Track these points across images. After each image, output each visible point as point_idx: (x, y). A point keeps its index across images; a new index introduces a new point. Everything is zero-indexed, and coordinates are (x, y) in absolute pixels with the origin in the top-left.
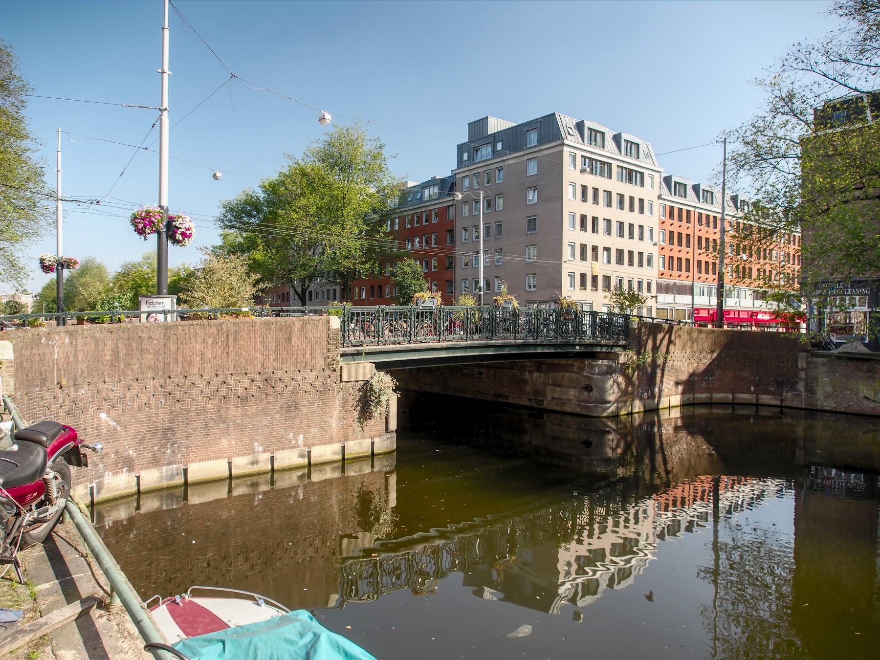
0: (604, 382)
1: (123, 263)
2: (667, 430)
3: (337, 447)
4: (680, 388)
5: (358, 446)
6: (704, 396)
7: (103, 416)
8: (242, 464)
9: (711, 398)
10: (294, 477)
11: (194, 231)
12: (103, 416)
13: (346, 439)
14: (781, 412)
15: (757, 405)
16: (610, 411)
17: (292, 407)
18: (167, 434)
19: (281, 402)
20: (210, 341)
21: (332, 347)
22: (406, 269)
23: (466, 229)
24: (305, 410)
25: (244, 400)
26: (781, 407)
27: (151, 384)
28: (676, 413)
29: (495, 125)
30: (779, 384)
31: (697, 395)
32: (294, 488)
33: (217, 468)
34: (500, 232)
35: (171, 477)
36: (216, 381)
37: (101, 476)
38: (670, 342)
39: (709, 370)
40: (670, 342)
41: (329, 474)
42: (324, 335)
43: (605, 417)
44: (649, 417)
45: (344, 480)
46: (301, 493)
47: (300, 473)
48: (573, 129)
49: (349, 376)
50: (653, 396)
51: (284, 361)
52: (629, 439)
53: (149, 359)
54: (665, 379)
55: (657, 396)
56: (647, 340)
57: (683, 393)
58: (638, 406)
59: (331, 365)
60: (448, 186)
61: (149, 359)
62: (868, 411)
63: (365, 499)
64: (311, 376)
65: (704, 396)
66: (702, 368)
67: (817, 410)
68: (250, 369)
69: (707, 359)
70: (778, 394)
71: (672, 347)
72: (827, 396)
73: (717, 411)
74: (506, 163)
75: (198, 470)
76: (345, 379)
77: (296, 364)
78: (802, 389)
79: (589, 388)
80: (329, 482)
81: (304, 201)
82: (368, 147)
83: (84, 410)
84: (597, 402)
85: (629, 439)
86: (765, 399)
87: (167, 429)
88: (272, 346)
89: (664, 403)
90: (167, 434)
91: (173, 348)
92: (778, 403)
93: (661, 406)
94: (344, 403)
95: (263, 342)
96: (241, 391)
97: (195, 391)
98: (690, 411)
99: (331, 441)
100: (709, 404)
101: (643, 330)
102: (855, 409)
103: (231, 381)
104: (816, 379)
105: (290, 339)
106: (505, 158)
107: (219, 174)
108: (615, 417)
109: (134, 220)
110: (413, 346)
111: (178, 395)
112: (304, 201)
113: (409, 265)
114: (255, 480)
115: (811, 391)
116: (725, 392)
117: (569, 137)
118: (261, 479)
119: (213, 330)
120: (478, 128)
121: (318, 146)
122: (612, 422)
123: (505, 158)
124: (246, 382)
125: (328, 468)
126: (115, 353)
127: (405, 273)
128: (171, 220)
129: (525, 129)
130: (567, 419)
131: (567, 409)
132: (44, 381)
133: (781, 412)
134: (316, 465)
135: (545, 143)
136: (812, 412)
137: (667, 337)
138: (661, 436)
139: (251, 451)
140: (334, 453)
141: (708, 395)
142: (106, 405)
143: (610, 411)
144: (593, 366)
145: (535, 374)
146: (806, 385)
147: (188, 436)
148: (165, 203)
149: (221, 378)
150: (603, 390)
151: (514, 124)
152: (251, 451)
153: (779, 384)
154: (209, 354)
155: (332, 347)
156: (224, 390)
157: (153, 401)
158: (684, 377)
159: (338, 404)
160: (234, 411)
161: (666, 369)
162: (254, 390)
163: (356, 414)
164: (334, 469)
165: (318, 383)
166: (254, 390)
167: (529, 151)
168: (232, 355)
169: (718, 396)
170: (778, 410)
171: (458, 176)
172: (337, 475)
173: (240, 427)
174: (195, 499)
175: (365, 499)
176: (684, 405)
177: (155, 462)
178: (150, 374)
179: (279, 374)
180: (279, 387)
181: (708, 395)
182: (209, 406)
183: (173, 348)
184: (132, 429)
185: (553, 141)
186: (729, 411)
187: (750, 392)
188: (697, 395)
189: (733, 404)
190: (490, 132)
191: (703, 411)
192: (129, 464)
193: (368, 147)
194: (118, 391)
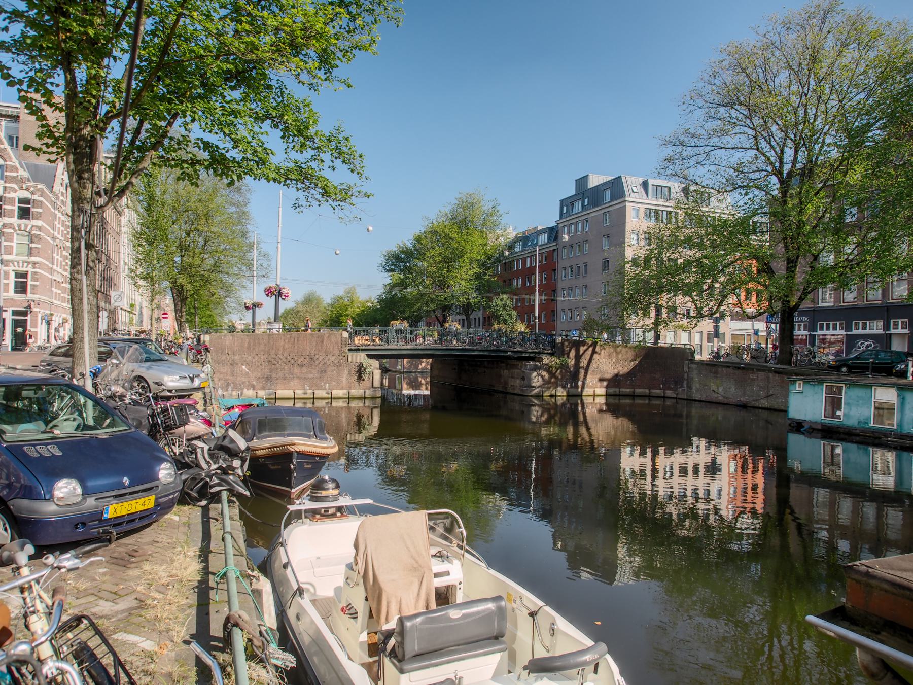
0: (531, 374)
1: (332, 296)
2: (591, 411)
3: (346, 391)
4: (605, 383)
5: (356, 392)
6: (628, 390)
7: (244, 367)
8: (299, 393)
9: (634, 392)
10: (324, 402)
11: (290, 295)
12: (244, 367)
13: (350, 388)
14: (677, 402)
15: (664, 397)
16: (534, 392)
17: (323, 372)
18: (268, 377)
19: (318, 369)
20: (287, 341)
21: (343, 346)
22: (499, 303)
23: (564, 269)
24: (329, 373)
25: (301, 366)
26: (676, 398)
27: (262, 357)
28: (601, 400)
29: (595, 181)
30: (676, 383)
31: (621, 390)
32: (324, 408)
33: (289, 393)
34: (586, 272)
35: (270, 395)
36: (289, 358)
37: (242, 390)
38: (594, 352)
39: (631, 374)
40: (594, 352)
41: (341, 404)
42: (340, 340)
43: (531, 396)
44: (573, 400)
45: (349, 408)
46: (326, 410)
47: (327, 401)
48: (638, 186)
49: (352, 359)
50: (577, 386)
51: (319, 351)
52: (552, 412)
53: (262, 347)
54: (589, 376)
55: (580, 387)
56: (570, 350)
57: (607, 387)
58: (561, 392)
59: (343, 354)
60: (553, 233)
61: (262, 347)
62: (714, 400)
63: (359, 417)
64: (333, 359)
65: (628, 390)
66: (626, 370)
67: (693, 400)
68: (304, 353)
69: (630, 366)
70: (675, 390)
71: (595, 356)
72: (698, 390)
73: (639, 401)
74: (591, 215)
75: (281, 393)
76: (350, 360)
77: (326, 352)
78: (685, 386)
79: (523, 379)
80: (342, 408)
81: (433, 253)
82: (486, 207)
83: (237, 364)
84: (527, 387)
85: (552, 412)
86: (669, 393)
87: (268, 376)
88: (314, 344)
89: (588, 391)
90: (268, 377)
91: (272, 343)
92: (675, 396)
93: (584, 394)
94: (350, 371)
95: (310, 342)
96: (300, 363)
97: (280, 361)
98: (611, 400)
99: (342, 388)
100: (633, 396)
101: (566, 343)
102: (709, 399)
103: (296, 358)
104: (692, 378)
105: (322, 342)
106: (589, 212)
107: (338, 252)
108: (539, 396)
109: (266, 290)
110: (389, 347)
111: (273, 362)
112: (433, 253)
113: (501, 300)
114: (305, 401)
115: (690, 387)
116: (644, 388)
117: (633, 195)
118: (308, 401)
119: (288, 336)
120: (582, 182)
121: (448, 209)
122: (535, 399)
123: (589, 212)
124: (302, 359)
125: (341, 401)
126: (249, 343)
127: (497, 306)
128: (281, 289)
129: (602, 188)
130: (516, 397)
131: (516, 392)
132: (222, 352)
133: (677, 402)
134: (335, 398)
135: (616, 200)
136: (690, 401)
137: (591, 349)
138: (584, 414)
139: (304, 388)
140: (344, 394)
141: (632, 390)
142: (245, 363)
143: (534, 392)
144: (526, 365)
145: (505, 371)
146: (687, 384)
147: (277, 379)
148: (278, 283)
149: (291, 356)
150: (530, 379)
151: (610, 178)
152: (304, 388)
153: (676, 383)
154: (286, 346)
155: (343, 346)
156: (292, 362)
157: (263, 364)
158: (609, 376)
159: (346, 372)
160: (296, 371)
161: (590, 372)
162: (305, 363)
163: (356, 378)
164: (344, 402)
165: (336, 362)
166: (305, 363)
167: (606, 206)
168: (296, 347)
169: (639, 391)
170: (674, 401)
171: (561, 225)
172: (345, 405)
173: (299, 378)
174: (279, 403)
175: (359, 417)
176: (607, 395)
177: (263, 388)
178: (262, 353)
179: (317, 356)
180: (317, 362)
181: (632, 390)
182: (286, 368)
183: (272, 343)
184: (255, 374)
185: (618, 199)
186: (647, 402)
187: (660, 389)
188: (621, 390)
189: (649, 397)
190: (590, 186)
191: (628, 401)
192: (253, 387)
193: (486, 207)
194: (249, 359)
